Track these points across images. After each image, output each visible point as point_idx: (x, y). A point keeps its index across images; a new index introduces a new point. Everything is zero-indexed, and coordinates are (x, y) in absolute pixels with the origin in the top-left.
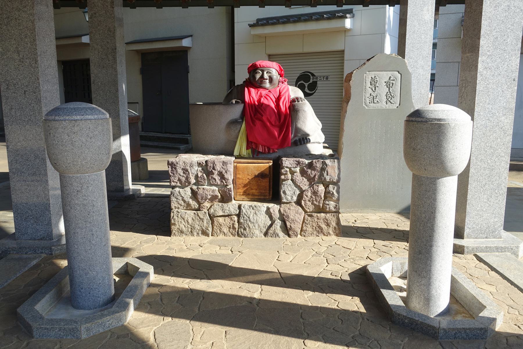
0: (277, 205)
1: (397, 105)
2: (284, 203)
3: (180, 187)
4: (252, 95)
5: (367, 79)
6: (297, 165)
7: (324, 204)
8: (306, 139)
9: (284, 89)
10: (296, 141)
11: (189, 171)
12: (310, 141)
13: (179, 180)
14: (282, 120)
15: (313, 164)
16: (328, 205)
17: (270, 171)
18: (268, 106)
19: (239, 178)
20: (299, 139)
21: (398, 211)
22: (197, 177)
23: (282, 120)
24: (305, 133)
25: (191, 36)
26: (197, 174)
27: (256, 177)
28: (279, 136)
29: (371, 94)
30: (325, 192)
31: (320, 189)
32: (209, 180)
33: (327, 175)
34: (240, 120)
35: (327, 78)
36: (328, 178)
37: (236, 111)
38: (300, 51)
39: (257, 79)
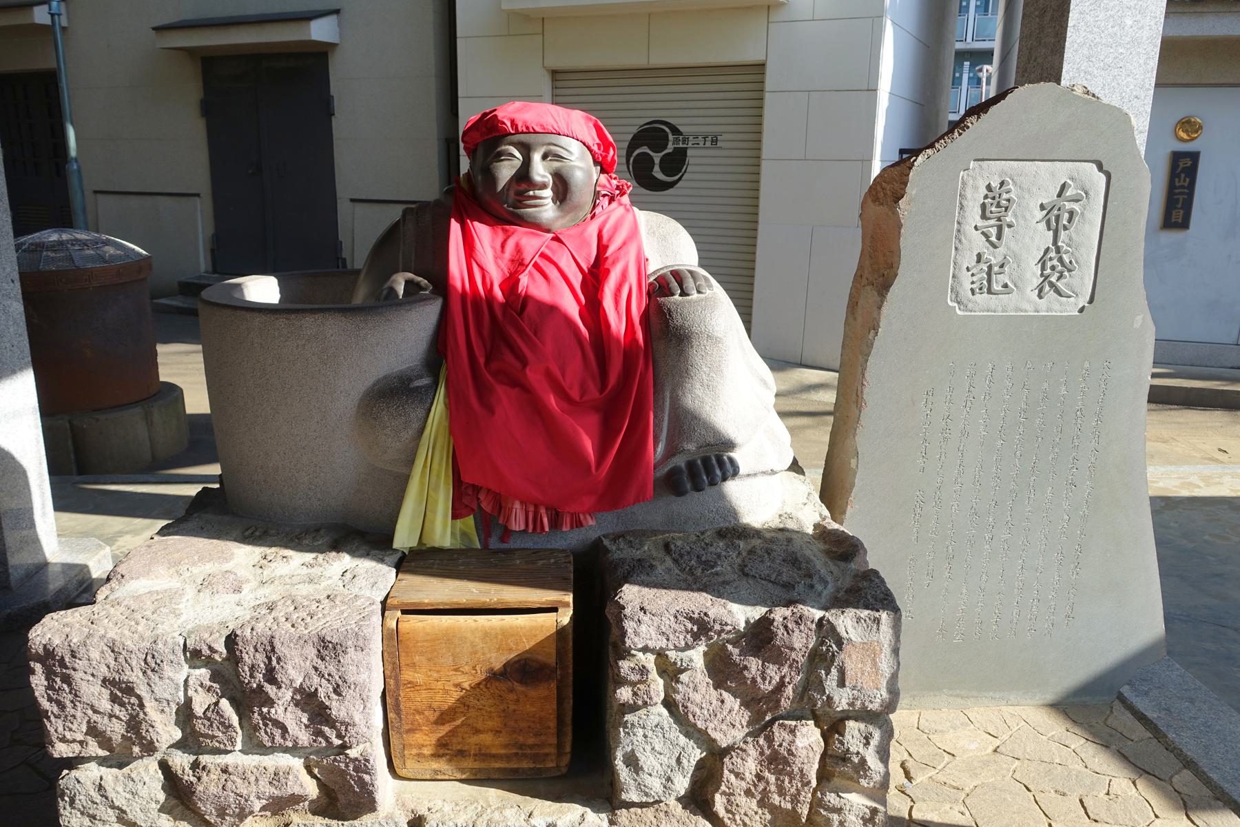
0: (597, 810)
1: (1083, 301)
2: (629, 805)
3: (102, 762)
4: (479, 256)
5: (969, 193)
6: (696, 637)
7: (816, 804)
8: (721, 463)
9: (616, 228)
10: (674, 474)
11: (142, 690)
12: (735, 473)
13: (93, 731)
14: (613, 379)
15: (771, 636)
16: (839, 811)
17: (560, 653)
18: (552, 310)
19: (413, 685)
20: (691, 465)
21: (1050, 697)
22: (185, 714)
23: (613, 379)
24: (716, 432)
25: (337, 12)
26: (188, 701)
27: (495, 677)
28: (602, 451)
29: (979, 256)
30: (824, 756)
31: (801, 742)
32: (251, 731)
33: (842, 683)
34: (425, 381)
35: (715, 141)
36: (842, 699)
37: (406, 337)
38: (639, 60)
39: (500, 188)
